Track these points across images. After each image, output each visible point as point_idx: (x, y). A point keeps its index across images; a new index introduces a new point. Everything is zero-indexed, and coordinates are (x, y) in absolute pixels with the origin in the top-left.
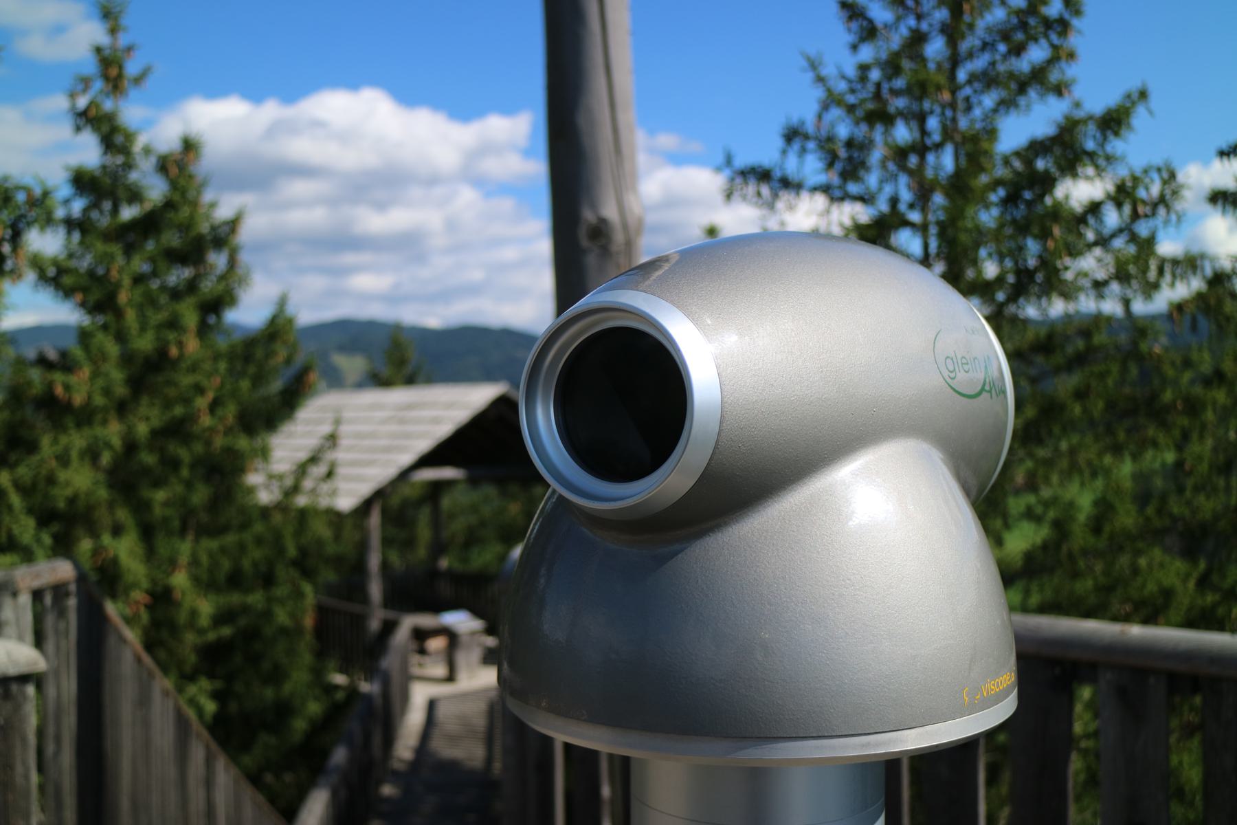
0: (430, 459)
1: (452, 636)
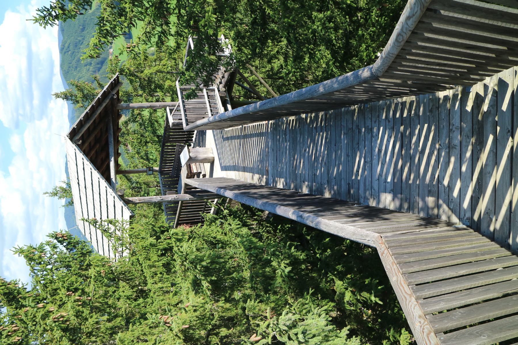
0: (105, 174)
1: (191, 160)
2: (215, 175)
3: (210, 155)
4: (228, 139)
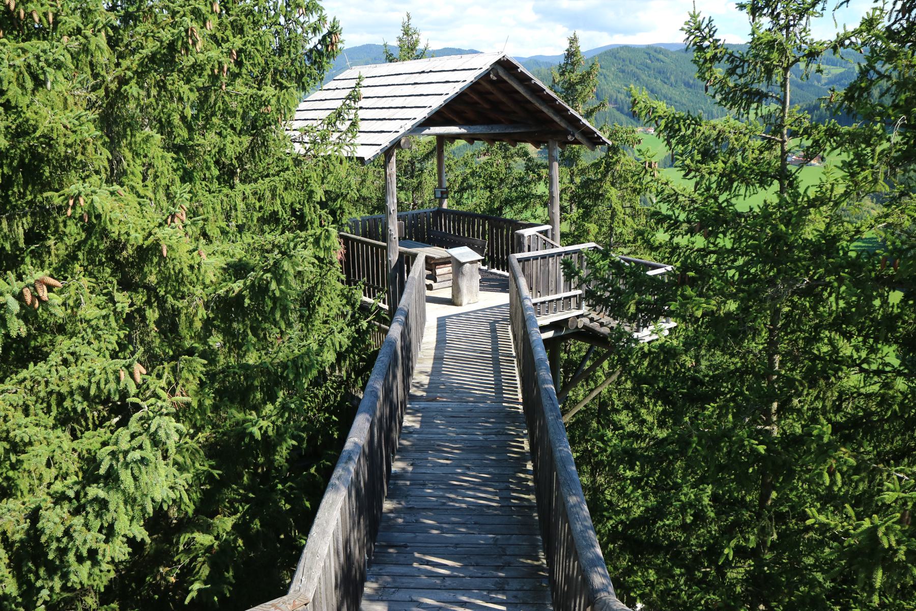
1: (458, 266)
2: (429, 306)
3: (465, 298)
4: (493, 330)
